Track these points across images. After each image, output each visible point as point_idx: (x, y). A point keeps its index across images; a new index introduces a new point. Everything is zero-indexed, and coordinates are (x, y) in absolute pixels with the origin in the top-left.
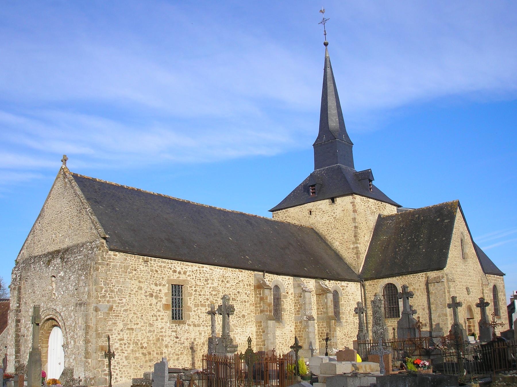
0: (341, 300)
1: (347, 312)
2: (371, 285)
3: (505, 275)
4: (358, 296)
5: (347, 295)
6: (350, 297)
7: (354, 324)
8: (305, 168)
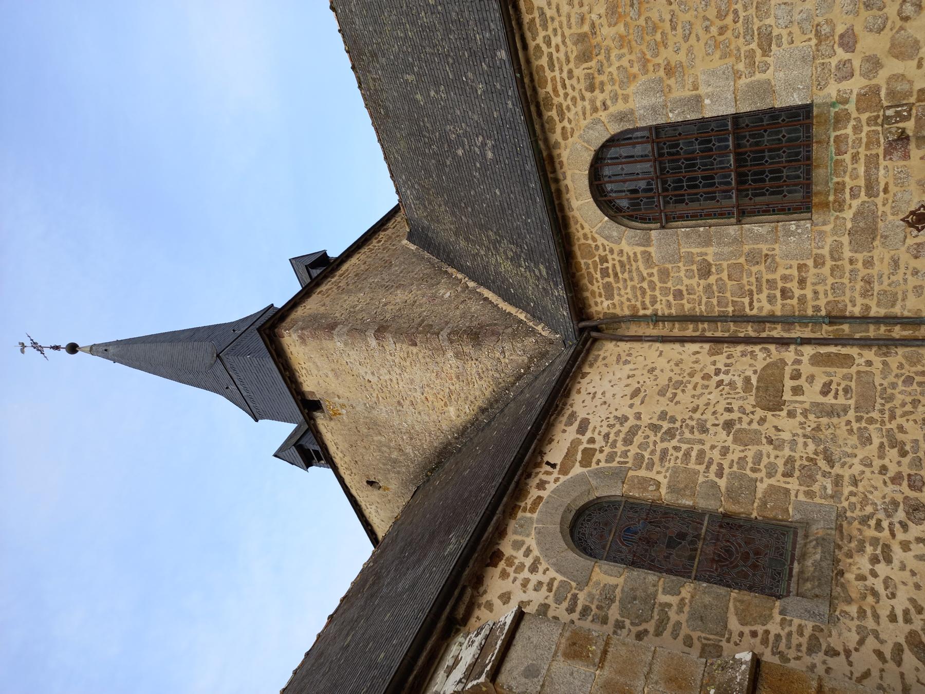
0: (644, 483)
1: (736, 453)
2: (608, 287)
3: (869, 670)
4: (661, 363)
5: (633, 431)
6: (649, 413)
7: (831, 412)
8: (609, 349)
